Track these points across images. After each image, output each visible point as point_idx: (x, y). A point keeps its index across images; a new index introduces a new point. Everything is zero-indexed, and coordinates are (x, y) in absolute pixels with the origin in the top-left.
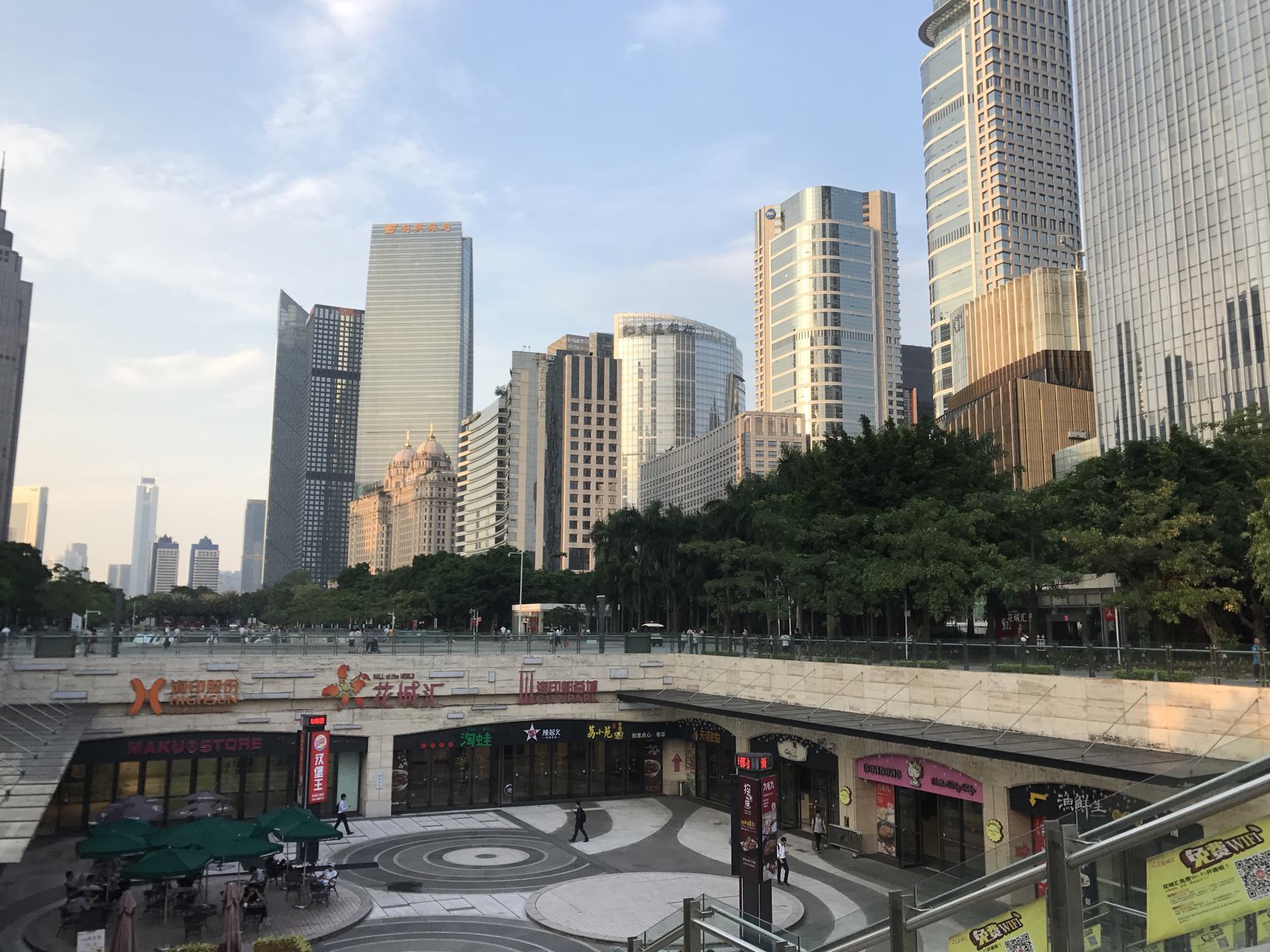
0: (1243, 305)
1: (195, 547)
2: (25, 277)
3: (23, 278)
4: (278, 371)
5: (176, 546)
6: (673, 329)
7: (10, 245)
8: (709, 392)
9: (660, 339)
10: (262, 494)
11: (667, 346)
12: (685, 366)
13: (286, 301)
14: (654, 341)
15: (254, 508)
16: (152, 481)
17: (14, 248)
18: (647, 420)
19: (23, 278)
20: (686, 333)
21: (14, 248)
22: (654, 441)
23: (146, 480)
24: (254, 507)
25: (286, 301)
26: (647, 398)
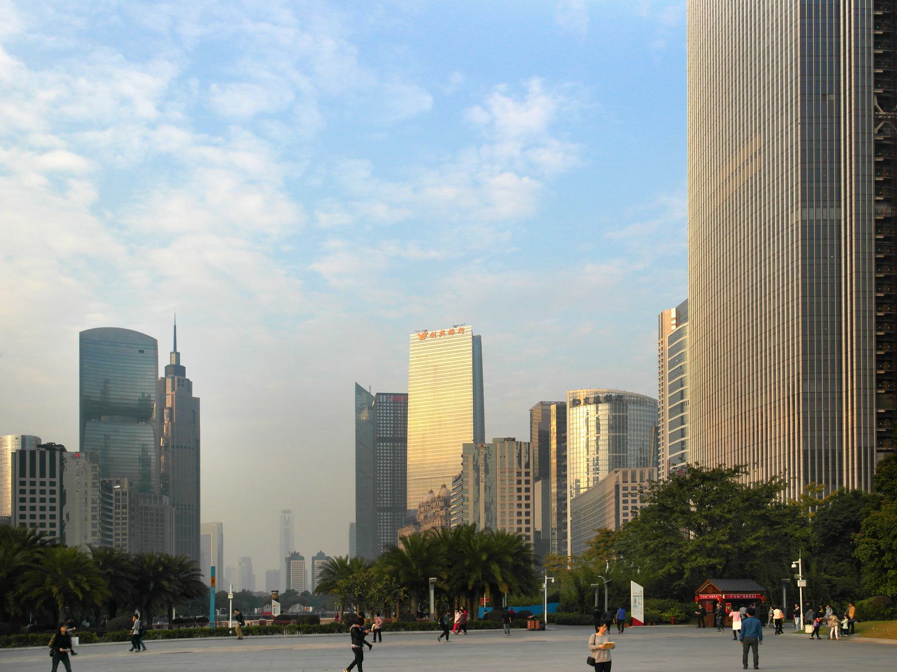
0: (818, 226)
1: (314, 559)
2: (194, 395)
3: (194, 395)
4: (356, 439)
5: (303, 558)
6: (608, 399)
7: (184, 375)
8: (635, 437)
9: (601, 407)
10: (354, 520)
11: (604, 408)
12: (618, 425)
13: (359, 390)
14: (597, 408)
15: (351, 525)
16: (289, 512)
17: (187, 377)
18: (593, 443)
19: (194, 395)
20: (618, 403)
21: (187, 377)
22: (597, 458)
23: (284, 512)
24: (351, 525)
25: (359, 390)
26: (593, 428)
